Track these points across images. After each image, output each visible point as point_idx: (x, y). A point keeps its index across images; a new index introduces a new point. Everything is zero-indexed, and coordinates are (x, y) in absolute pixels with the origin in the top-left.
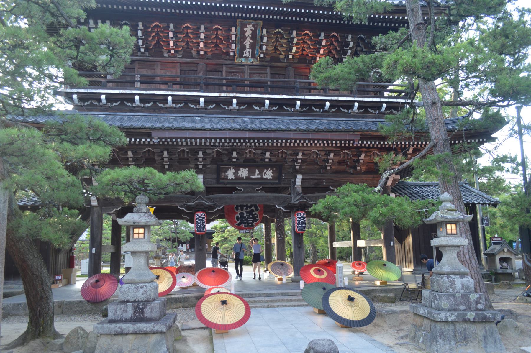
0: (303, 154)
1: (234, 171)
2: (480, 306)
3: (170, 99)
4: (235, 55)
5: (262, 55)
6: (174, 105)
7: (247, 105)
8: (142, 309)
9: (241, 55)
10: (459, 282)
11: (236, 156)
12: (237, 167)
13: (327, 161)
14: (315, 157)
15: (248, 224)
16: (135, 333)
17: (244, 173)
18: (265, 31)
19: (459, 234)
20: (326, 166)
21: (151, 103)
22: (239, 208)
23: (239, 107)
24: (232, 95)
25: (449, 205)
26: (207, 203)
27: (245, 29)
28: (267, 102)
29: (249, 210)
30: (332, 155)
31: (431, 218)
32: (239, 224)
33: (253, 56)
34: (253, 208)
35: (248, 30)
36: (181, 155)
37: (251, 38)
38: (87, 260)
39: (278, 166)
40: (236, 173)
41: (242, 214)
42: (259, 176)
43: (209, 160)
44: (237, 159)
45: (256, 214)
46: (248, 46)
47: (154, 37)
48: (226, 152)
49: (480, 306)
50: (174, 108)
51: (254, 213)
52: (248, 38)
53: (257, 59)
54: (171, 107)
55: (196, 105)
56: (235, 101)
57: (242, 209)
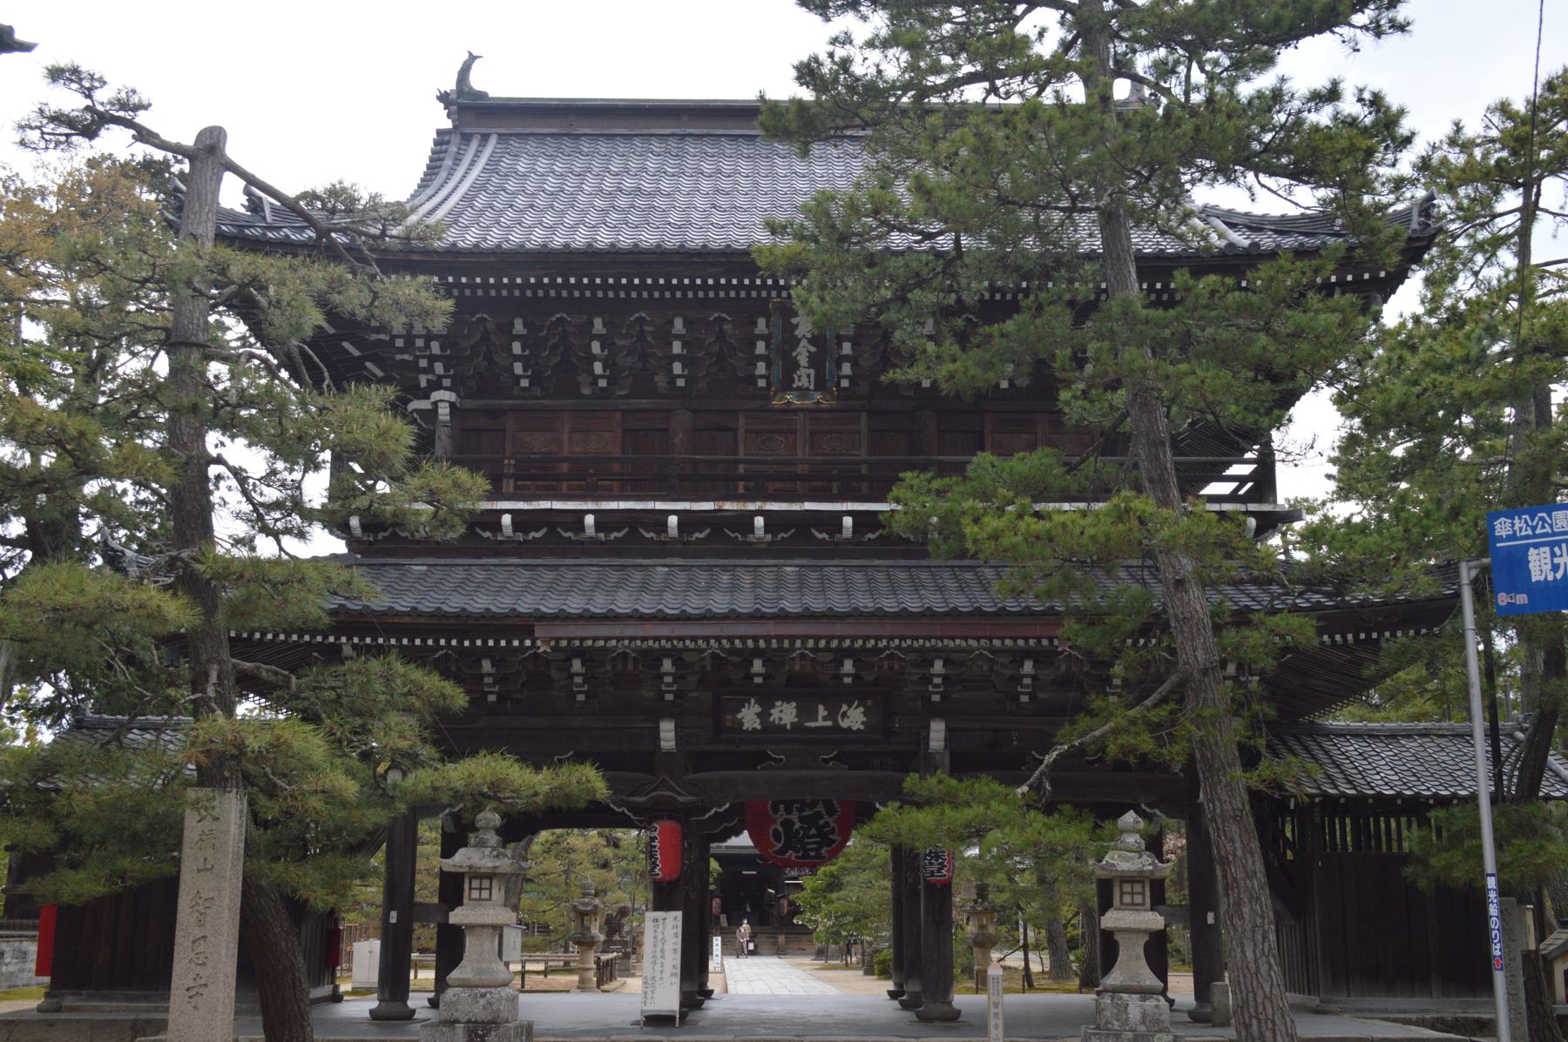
0: (947, 663)
1: (758, 709)
3: (589, 520)
4: (769, 384)
6: (602, 535)
9: (787, 385)
11: (763, 670)
12: (767, 698)
14: (986, 667)
15: (806, 851)
17: (785, 713)
19: (1148, 905)
21: (544, 530)
22: (782, 806)
23: (774, 535)
24: (751, 506)
26: (681, 799)
29: (808, 812)
30: (1028, 667)
32: (782, 851)
33: (820, 384)
34: (820, 808)
36: (620, 667)
37: (812, 341)
38: (376, 944)
40: (763, 715)
41: (787, 824)
42: (829, 723)
44: (766, 677)
45: (827, 824)
46: (803, 360)
47: (555, 346)
48: (737, 659)
50: (602, 543)
51: (821, 822)
52: (804, 342)
53: (831, 392)
54: (592, 540)
55: (658, 533)
56: (759, 521)
57: (789, 811)
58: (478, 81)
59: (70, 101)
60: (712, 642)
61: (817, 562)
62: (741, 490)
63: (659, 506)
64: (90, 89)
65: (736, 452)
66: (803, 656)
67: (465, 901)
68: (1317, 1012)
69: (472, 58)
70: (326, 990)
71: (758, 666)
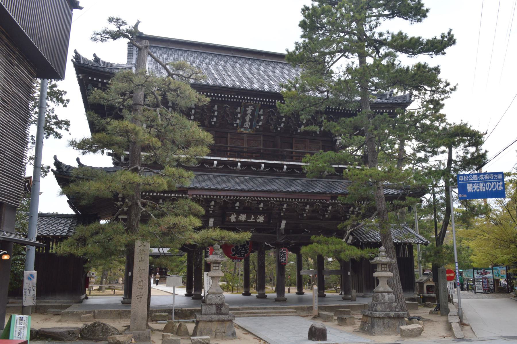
1: (236, 216)
2: (397, 310)
5: (258, 127)
7: (247, 168)
8: (220, 308)
9: (242, 126)
10: (387, 296)
12: (238, 214)
13: (304, 210)
16: (218, 321)
17: (243, 217)
18: (262, 111)
20: (303, 214)
24: (237, 160)
25: (383, 254)
27: (247, 109)
28: (263, 165)
30: (308, 207)
31: (374, 261)
32: (234, 255)
33: (251, 127)
35: (249, 110)
37: (251, 115)
39: (267, 212)
40: (237, 218)
43: (217, 207)
46: (248, 120)
49: (397, 310)
52: (249, 115)
53: (254, 129)
56: (239, 164)
58: (140, 29)
59: (113, 28)
60: (271, 199)
61: (254, 176)
62: (229, 155)
63: (212, 158)
64: (121, 25)
65: (227, 144)
66: (248, 202)
67: (212, 270)
68: (363, 297)
69: (139, 22)
70: (84, 296)
71: (238, 204)
